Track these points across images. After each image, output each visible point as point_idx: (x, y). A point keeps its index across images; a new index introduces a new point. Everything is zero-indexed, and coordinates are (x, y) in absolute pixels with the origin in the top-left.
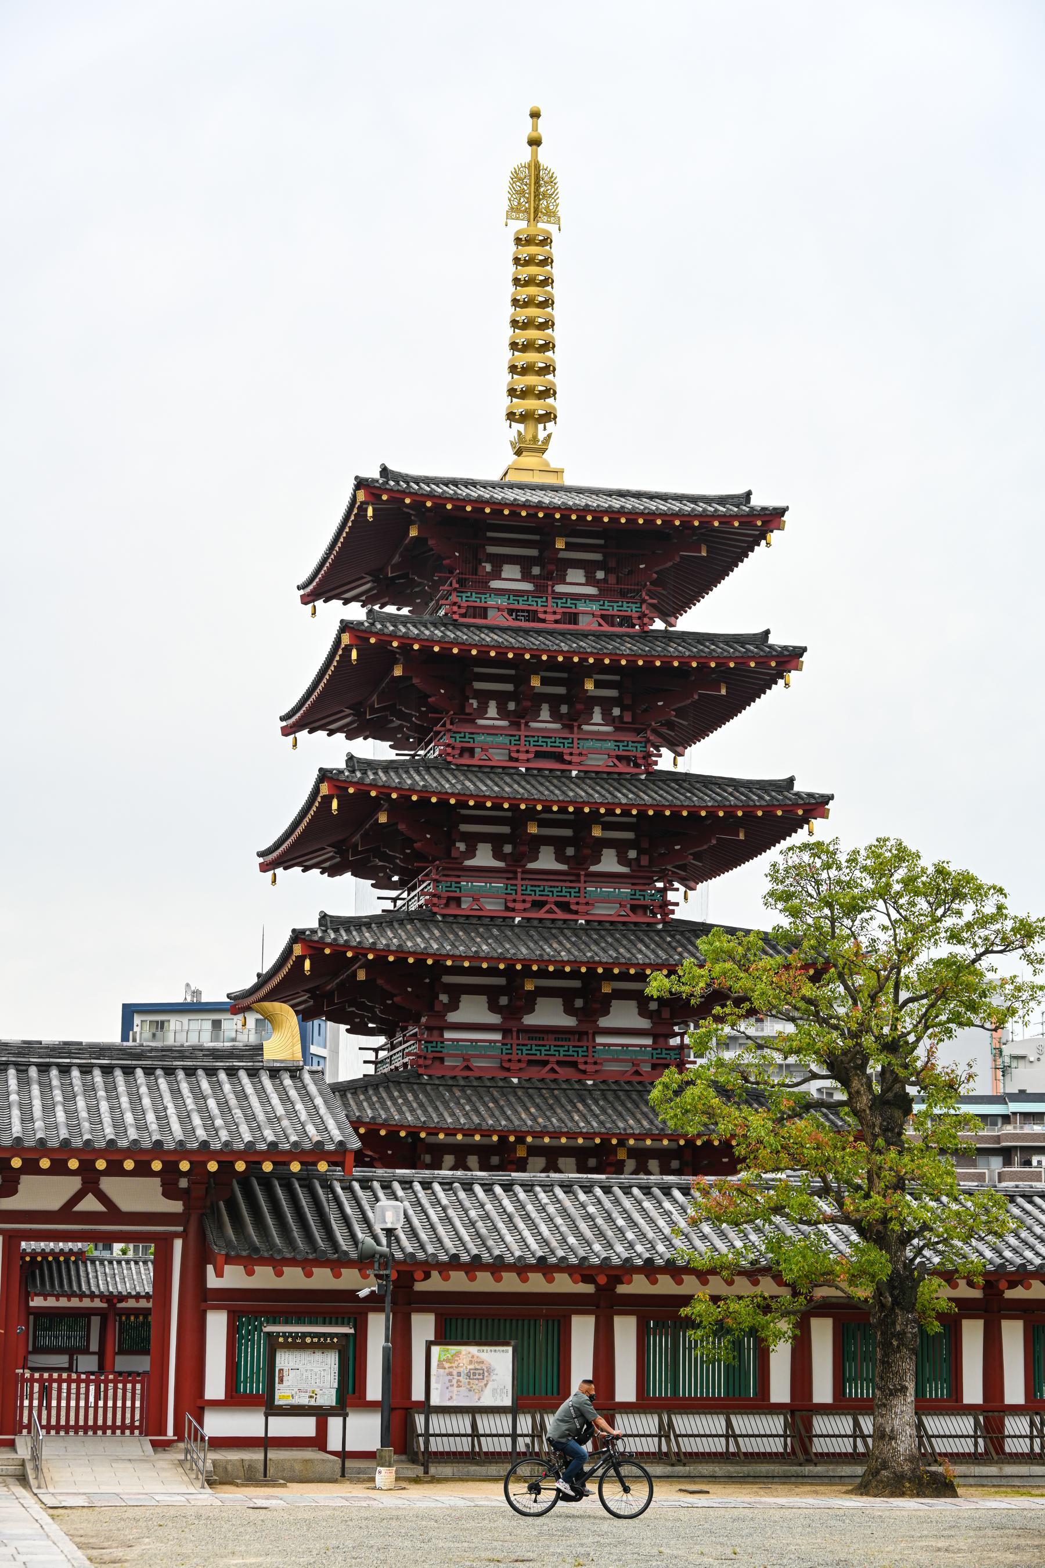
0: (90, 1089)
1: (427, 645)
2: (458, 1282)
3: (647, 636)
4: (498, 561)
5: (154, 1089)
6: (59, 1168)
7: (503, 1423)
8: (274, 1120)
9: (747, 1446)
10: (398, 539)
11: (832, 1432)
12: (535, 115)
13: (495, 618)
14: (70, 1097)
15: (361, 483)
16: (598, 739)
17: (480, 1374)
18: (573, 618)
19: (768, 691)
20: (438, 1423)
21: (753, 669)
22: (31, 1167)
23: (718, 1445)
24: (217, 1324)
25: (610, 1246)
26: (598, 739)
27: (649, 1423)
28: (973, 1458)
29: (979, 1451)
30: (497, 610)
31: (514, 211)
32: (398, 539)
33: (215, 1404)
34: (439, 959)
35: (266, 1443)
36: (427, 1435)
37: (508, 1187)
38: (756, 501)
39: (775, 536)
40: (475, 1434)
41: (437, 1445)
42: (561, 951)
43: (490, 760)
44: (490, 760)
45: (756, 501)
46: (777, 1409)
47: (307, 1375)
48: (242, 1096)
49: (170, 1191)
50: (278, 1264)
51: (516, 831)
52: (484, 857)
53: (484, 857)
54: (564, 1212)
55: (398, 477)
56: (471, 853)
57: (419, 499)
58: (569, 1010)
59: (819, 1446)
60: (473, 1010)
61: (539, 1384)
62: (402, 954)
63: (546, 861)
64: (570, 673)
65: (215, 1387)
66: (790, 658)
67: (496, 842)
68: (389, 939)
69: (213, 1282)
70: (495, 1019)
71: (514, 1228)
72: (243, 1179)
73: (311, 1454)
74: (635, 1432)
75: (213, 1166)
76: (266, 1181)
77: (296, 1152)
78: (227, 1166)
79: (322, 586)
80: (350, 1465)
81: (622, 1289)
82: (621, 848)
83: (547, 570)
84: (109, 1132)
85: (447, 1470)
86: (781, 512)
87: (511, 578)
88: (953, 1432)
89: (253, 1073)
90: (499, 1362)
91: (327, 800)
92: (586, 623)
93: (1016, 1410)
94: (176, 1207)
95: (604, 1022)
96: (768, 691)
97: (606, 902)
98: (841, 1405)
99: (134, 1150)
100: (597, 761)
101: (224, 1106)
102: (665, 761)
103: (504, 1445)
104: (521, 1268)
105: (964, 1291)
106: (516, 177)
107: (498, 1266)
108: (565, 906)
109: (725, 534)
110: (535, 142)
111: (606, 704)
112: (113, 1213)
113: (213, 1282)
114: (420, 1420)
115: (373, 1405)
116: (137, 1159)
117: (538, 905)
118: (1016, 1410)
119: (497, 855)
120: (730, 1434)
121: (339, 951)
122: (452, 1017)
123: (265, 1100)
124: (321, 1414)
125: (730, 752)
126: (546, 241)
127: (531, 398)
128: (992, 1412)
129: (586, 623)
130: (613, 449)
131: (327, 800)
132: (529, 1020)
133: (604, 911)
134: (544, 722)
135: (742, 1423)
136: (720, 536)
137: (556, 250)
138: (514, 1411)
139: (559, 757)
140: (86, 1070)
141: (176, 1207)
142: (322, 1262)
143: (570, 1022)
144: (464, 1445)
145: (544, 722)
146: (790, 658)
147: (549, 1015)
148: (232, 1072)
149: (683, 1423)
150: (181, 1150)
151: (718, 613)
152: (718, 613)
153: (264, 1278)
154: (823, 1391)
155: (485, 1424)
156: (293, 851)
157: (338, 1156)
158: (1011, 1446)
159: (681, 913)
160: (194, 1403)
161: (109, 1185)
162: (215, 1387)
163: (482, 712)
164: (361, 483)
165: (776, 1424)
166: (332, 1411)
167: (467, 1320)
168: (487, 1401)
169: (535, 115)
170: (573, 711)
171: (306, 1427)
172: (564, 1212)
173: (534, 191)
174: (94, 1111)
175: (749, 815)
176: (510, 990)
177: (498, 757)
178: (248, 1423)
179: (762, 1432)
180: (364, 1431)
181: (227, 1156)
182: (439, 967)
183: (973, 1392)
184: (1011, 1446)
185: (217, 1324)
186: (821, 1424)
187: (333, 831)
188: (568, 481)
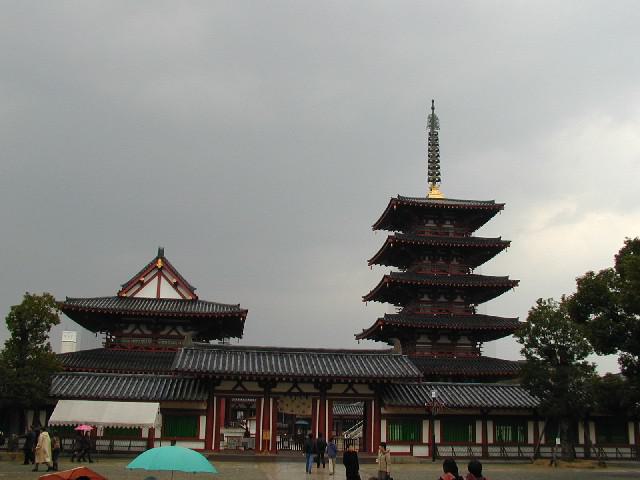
6: (288, 381)
10: (400, 214)
19: (618, 254)
21: (496, 246)
22: (281, 380)
24: (384, 424)
27: (498, 449)
29: (98, 442)
46: (530, 445)
49: (316, 387)
51: (434, 291)
52: (426, 298)
53: (426, 298)
60: (423, 339)
63: (442, 299)
66: (515, 283)
69: (383, 411)
70: (429, 341)
74: (494, 451)
79: (378, 226)
84: (251, 370)
86: (503, 205)
87: (431, 224)
92: (451, 235)
94: (372, 392)
95: (459, 342)
96: (618, 254)
97: (458, 310)
98: (495, 444)
99: (287, 376)
104: (464, 408)
107: (459, 407)
108: (447, 311)
109: (488, 211)
110: (433, 108)
112: (246, 391)
115: (425, 444)
116: (252, 377)
117: (440, 311)
119: (429, 297)
125: (488, 269)
127: (434, 176)
128: (485, 445)
129: (451, 235)
130: (456, 188)
132: (439, 341)
134: (441, 262)
136: (486, 211)
141: (372, 392)
143: (449, 342)
146: (515, 283)
151: (484, 232)
152: (484, 232)
154: (490, 440)
163: (438, 260)
165: (531, 449)
173: (433, 122)
175: (401, 283)
179: (528, 451)
185: (384, 424)
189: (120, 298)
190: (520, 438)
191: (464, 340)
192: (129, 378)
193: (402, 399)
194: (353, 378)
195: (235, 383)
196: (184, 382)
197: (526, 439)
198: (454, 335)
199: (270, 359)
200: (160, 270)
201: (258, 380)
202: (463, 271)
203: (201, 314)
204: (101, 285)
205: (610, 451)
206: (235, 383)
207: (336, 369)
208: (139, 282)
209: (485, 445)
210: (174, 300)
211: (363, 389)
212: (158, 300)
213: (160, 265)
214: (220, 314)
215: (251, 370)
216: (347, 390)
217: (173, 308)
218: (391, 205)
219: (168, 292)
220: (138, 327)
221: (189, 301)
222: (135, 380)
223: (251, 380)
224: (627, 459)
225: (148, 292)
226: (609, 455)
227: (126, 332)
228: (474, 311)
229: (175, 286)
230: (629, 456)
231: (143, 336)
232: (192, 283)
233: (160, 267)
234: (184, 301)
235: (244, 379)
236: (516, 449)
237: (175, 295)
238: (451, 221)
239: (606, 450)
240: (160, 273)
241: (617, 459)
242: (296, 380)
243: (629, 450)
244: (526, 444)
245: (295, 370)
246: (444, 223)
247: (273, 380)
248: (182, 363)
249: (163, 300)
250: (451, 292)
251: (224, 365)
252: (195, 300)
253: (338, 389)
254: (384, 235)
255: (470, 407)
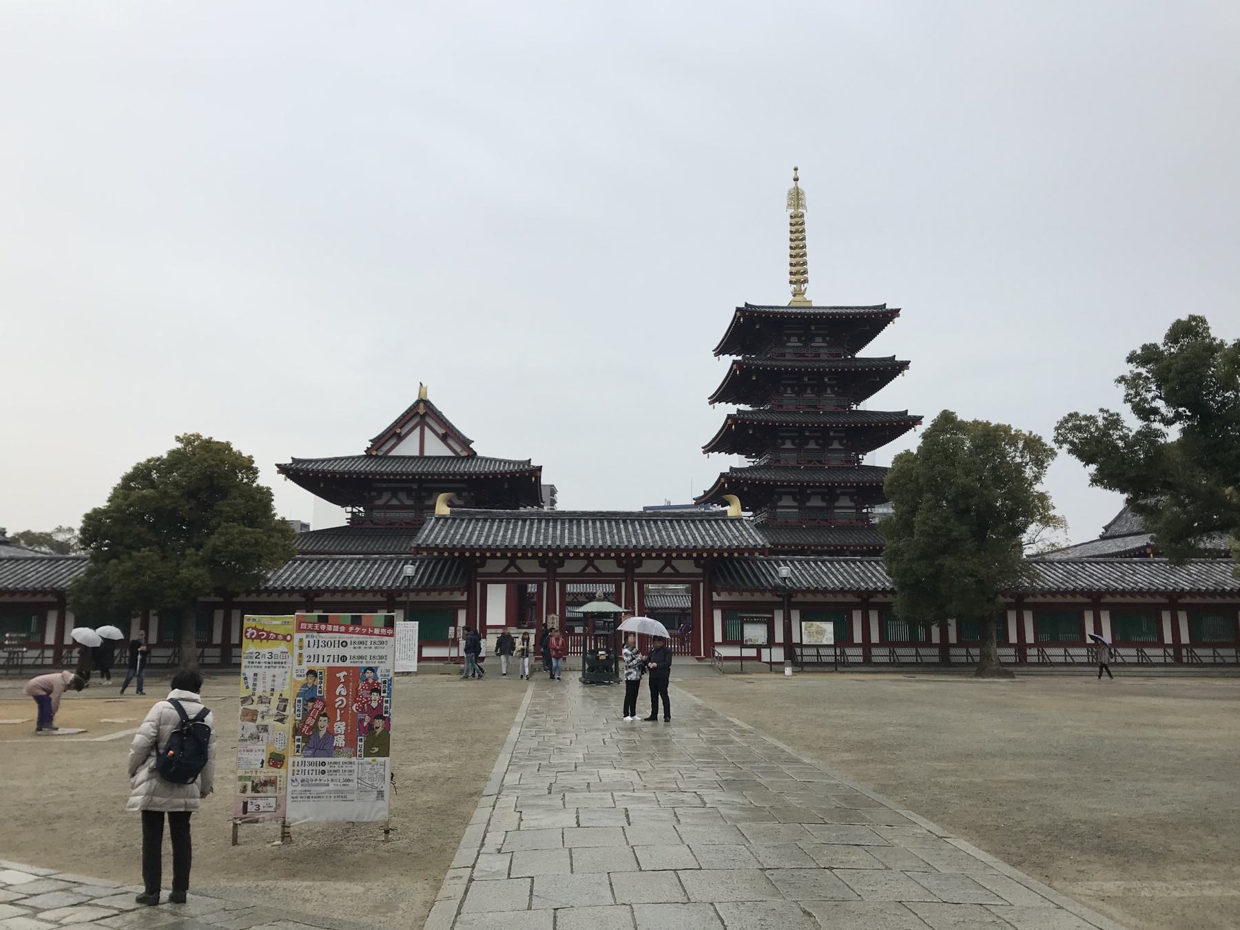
0: (666, 528)
1: (765, 367)
2: (810, 598)
3: (846, 359)
4: (789, 336)
5: (689, 527)
7: (831, 652)
8: (735, 538)
9: (925, 660)
10: (751, 331)
11: (958, 654)
12: (796, 169)
13: (788, 357)
14: (659, 531)
15: (738, 309)
16: (830, 400)
17: (821, 632)
18: (818, 355)
20: (805, 652)
21: (890, 369)
23: (913, 659)
24: (718, 615)
25: (866, 583)
26: (830, 400)
27: (885, 651)
28: (1015, 664)
30: (790, 355)
31: (789, 206)
32: (751, 331)
33: (719, 644)
34: (775, 482)
35: (741, 658)
36: (802, 655)
37: (823, 562)
38: (888, 307)
39: (896, 319)
40: (818, 655)
41: (806, 659)
42: (821, 477)
43: (790, 408)
44: (790, 408)
45: (888, 307)
46: (858, 645)
47: (755, 633)
48: (722, 530)
50: (741, 591)
51: (799, 434)
52: (788, 445)
53: (788, 445)
54: (846, 571)
55: (752, 306)
56: (783, 443)
57: (760, 313)
58: (823, 500)
59: (874, 659)
60: (787, 501)
61: (843, 638)
62: (761, 480)
63: (812, 445)
64: (817, 375)
65: (718, 638)
67: (793, 439)
68: (756, 475)
69: (716, 597)
70: (796, 504)
71: (828, 578)
72: (738, 560)
73: (756, 663)
74: (880, 655)
75: (467, 554)
76: (746, 560)
77: (747, 549)
78: (721, 555)
79: (722, 350)
80: (773, 666)
81: (871, 600)
82: (840, 440)
83: (807, 338)
85: (809, 669)
87: (794, 342)
88: (1007, 655)
89: (724, 521)
90: (828, 627)
91: (730, 426)
93: (1031, 646)
94: (700, 571)
95: (837, 504)
97: (836, 460)
98: (959, 645)
99: (686, 549)
100: (830, 408)
101: (716, 532)
102: (854, 408)
103: (832, 659)
104: (834, 592)
105: (1009, 600)
106: (790, 193)
108: (820, 462)
110: (796, 180)
111: (832, 387)
112: (677, 573)
113: (716, 597)
114: (798, 651)
115: (779, 645)
117: (810, 461)
118: (1031, 646)
119: (793, 443)
120: (918, 654)
121: (738, 480)
122: (779, 504)
123: (730, 530)
124: (759, 648)
125: (880, 402)
126: (802, 216)
127: (799, 274)
128: (1021, 646)
130: (829, 291)
131: (730, 426)
132: (808, 504)
133: (834, 463)
134: (809, 395)
135: (922, 651)
136: (876, 320)
137: (806, 219)
138: (834, 647)
139: (815, 407)
140: (663, 522)
142: (756, 591)
143: (824, 504)
144: (814, 659)
145: (809, 395)
147: (816, 502)
148: (716, 521)
149: (899, 651)
150: (704, 549)
151: (873, 350)
152: (873, 350)
153: (735, 597)
154: (1030, 638)
155: (822, 652)
156: (716, 446)
157: (763, 550)
158: (1029, 660)
159: (864, 463)
160: (710, 643)
161: (675, 563)
162: (718, 638)
163: (785, 392)
164: (738, 309)
166: (765, 647)
167: (812, 612)
168: (825, 642)
169: (796, 169)
170: (820, 390)
171: (752, 652)
172: (846, 571)
173: (796, 198)
174: (669, 536)
176: (800, 493)
177: (792, 408)
178: (734, 652)
179: (931, 654)
180: (778, 655)
181: (721, 550)
182: (775, 485)
183: (1013, 638)
184: (1029, 660)
185: (718, 615)
186: (953, 651)
187: (724, 442)
188: (814, 305)
189: (369, 455)
190: (922, 636)
191: (845, 501)
192: (359, 560)
193: (734, 579)
194: (670, 550)
195: (585, 562)
196: (452, 565)
197: (211, 639)
198: (830, 493)
199: (555, 528)
200: (423, 416)
201: (617, 557)
202: (841, 407)
203: (478, 475)
204: (346, 441)
205: (1055, 653)
206: (585, 562)
207: (645, 539)
208: (394, 433)
209: (866, 644)
210: (444, 458)
211: (686, 567)
212: (422, 458)
213: (422, 410)
214: (503, 474)
215: (642, 543)
216: (664, 568)
217: (442, 468)
218: (736, 319)
219: (435, 447)
220: (395, 495)
221: (463, 458)
222: (365, 564)
223: (607, 557)
224: (1131, 664)
225: (408, 447)
226: (1054, 659)
227: (379, 502)
228: (858, 460)
229: (444, 438)
230: (1085, 660)
231: (403, 507)
232: (467, 434)
233: (422, 414)
234: (458, 458)
235: (597, 557)
236: (912, 651)
237: (443, 450)
238: (824, 336)
239: (1049, 651)
240: (422, 423)
241: (1066, 664)
242: (591, 555)
243: (1084, 651)
244: (928, 643)
245: (587, 540)
246: (813, 341)
247: (638, 556)
248: (428, 536)
249: (429, 458)
250: (823, 435)
251: (521, 537)
252: (473, 455)
253: (650, 567)
254: (727, 360)
255: (842, 591)
